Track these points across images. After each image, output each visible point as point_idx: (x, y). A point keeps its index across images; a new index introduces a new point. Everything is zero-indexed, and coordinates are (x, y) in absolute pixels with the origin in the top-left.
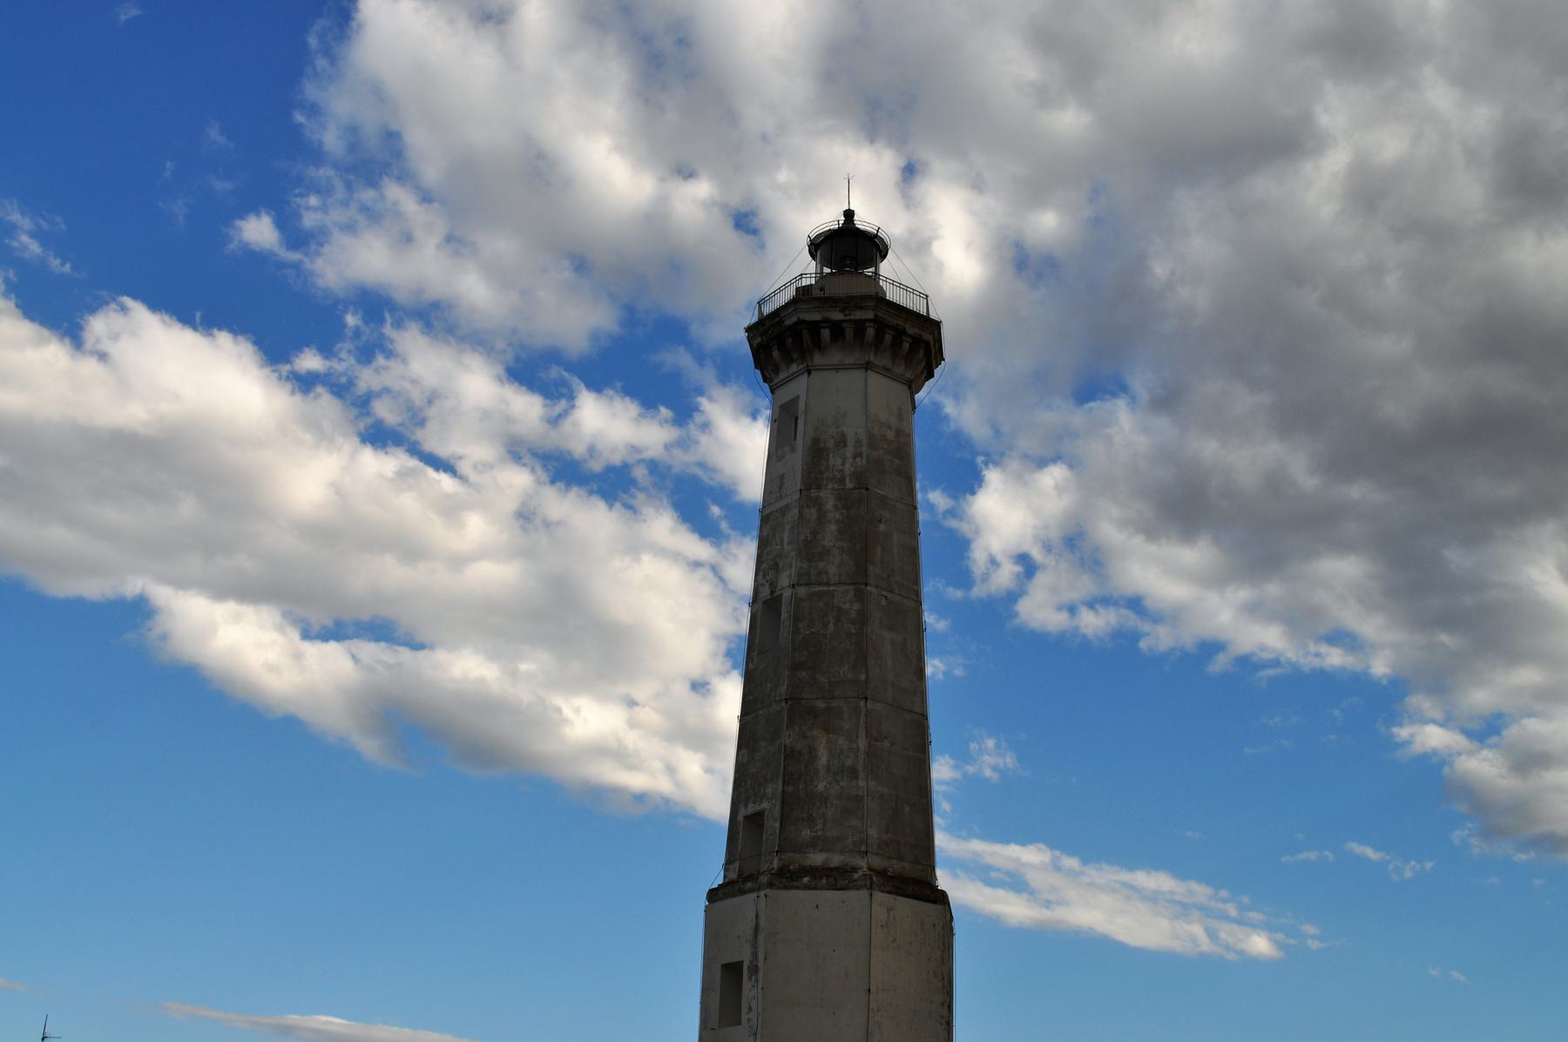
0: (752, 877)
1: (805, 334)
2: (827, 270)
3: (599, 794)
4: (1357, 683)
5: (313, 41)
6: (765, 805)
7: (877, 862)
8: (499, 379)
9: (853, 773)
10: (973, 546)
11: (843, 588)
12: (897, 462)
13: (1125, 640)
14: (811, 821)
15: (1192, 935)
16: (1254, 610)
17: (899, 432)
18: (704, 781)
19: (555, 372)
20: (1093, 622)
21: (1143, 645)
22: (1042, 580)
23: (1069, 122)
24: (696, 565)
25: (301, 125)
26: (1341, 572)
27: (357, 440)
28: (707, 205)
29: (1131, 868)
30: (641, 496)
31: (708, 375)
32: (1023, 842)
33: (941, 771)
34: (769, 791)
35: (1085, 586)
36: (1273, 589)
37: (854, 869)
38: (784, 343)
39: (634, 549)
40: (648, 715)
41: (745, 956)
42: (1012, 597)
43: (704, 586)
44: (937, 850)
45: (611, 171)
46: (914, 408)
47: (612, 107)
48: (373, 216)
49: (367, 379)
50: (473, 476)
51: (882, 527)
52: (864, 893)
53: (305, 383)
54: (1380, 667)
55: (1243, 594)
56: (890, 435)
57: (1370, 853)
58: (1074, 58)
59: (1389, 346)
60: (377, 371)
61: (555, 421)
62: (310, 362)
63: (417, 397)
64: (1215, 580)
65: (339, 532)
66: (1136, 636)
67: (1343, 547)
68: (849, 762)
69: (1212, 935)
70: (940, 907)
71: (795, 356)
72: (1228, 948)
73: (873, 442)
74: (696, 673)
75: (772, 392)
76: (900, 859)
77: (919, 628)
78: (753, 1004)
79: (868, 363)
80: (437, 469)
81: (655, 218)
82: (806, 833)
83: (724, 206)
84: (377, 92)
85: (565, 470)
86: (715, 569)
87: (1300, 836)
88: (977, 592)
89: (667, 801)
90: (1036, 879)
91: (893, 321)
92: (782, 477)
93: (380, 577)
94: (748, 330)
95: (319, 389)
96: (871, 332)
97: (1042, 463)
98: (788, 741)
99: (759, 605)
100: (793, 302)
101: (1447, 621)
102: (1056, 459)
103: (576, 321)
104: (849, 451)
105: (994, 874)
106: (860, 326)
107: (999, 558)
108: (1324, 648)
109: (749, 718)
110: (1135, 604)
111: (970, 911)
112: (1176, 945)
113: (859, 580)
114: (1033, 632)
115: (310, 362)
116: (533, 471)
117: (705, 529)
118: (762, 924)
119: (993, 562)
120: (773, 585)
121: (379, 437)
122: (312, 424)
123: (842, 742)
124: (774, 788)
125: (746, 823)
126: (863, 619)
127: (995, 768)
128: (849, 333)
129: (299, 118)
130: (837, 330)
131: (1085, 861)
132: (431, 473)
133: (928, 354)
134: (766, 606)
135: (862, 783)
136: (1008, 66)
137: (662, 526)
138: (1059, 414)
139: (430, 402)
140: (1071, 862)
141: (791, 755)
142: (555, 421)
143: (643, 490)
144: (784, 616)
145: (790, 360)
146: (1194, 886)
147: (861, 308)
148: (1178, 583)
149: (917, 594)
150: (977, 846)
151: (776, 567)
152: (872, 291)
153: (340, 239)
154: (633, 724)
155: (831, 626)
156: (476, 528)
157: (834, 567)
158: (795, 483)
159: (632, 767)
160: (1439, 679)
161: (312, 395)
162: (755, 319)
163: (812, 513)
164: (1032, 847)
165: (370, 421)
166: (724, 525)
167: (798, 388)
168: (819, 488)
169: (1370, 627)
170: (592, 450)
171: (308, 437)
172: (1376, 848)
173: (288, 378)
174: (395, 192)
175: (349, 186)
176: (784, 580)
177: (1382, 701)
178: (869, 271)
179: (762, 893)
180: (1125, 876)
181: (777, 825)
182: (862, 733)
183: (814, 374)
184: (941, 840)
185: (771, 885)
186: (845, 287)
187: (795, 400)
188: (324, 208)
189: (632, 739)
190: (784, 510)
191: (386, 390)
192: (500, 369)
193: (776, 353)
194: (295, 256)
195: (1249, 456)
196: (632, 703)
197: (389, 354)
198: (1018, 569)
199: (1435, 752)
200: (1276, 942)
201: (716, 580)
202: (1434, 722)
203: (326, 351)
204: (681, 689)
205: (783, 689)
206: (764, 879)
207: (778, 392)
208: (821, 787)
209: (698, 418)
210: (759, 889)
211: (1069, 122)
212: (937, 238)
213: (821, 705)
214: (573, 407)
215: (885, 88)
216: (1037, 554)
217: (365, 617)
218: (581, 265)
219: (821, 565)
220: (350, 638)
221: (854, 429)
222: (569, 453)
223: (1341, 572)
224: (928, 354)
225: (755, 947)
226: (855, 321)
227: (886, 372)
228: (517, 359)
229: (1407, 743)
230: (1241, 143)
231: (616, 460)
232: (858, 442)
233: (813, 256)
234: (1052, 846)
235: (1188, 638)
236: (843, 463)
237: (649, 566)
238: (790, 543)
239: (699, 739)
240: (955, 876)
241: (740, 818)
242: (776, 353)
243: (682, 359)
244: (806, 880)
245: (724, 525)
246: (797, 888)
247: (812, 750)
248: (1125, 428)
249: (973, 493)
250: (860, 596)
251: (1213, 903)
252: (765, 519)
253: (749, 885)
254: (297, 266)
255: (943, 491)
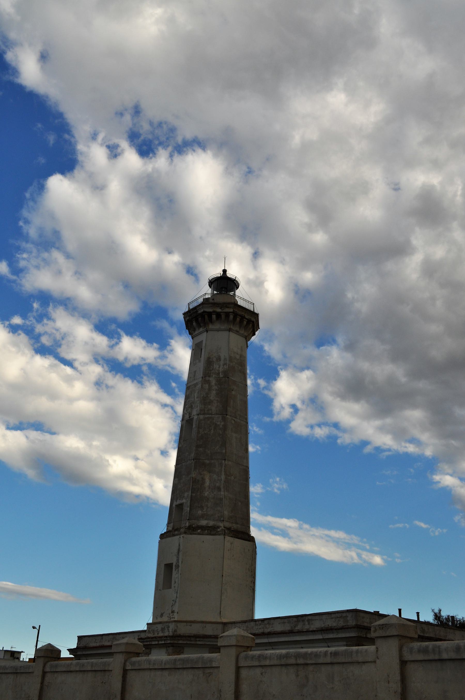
0: (177, 530)
1: (206, 317)
2: (215, 292)
3: (122, 494)
4: (420, 458)
5: (28, 195)
6: (184, 501)
7: (227, 525)
8: (91, 330)
9: (219, 489)
10: (275, 400)
11: (217, 416)
12: (240, 368)
13: (332, 439)
14: (202, 508)
15: (351, 556)
16: (381, 429)
17: (241, 356)
18: (161, 490)
19: (113, 327)
20: (320, 432)
21: (339, 441)
22: (301, 415)
23: (319, 238)
24: (165, 406)
25: (21, 227)
26: (415, 414)
27: (33, 352)
28: (176, 264)
29: (329, 529)
30: (145, 378)
31: (173, 331)
32: (288, 518)
33: (255, 489)
34: (186, 495)
35: (317, 418)
36: (389, 421)
37: (218, 527)
38: (198, 319)
39: (141, 398)
40: (142, 464)
41: (174, 561)
42: (289, 421)
43: (168, 413)
44: (251, 520)
45: (141, 249)
46: (247, 347)
47: (142, 225)
48: (47, 263)
49: (39, 328)
50: (80, 368)
51: (233, 393)
52: (222, 537)
53: (14, 329)
54: (428, 452)
55: (378, 423)
56: (238, 357)
57: (423, 525)
58: (322, 213)
59: (434, 328)
60: (43, 325)
61: (112, 347)
62: (17, 320)
63: (58, 337)
64: (367, 417)
65: (25, 387)
66: (336, 438)
67: (414, 406)
68: (217, 485)
69: (359, 555)
70: (251, 543)
71: (202, 325)
72: (365, 561)
73: (231, 359)
74: (162, 447)
75: (192, 338)
76: (237, 523)
77: (246, 433)
78: (177, 580)
79: (230, 329)
80: (65, 365)
81: (157, 269)
82: (200, 512)
83: (183, 264)
84: (52, 216)
85: (116, 366)
86: (172, 408)
87: (396, 518)
88: (275, 419)
89: (148, 498)
90: (292, 533)
91: (240, 313)
92: (195, 372)
93: (40, 405)
94: (184, 314)
95: (20, 332)
96: (231, 317)
97: (302, 369)
98: (194, 476)
99: (185, 422)
100: (202, 304)
101: (454, 435)
102: (308, 368)
103: (123, 308)
104: (222, 362)
105: (275, 530)
106: (227, 314)
107: (284, 406)
108: (407, 445)
109: (179, 466)
110: (336, 425)
111: (263, 543)
112: (345, 560)
113: (224, 413)
114: (297, 435)
115: (17, 320)
116: (103, 367)
117: (169, 391)
118: (181, 548)
119: (282, 407)
120: (190, 414)
121: (42, 351)
122: (15, 344)
123: (215, 476)
124: (188, 494)
125: (176, 508)
126: (225, 428)
127: (278, 489)
128: (223, 316)
129: (21, 223)
130: (218, 316)
131: (312, 526)
132: (62, 366)
133: (253, 326)
134: (187, 424)
135: (222, 493)
136: (297, 216)
137: (153, 389)
138: (311, 351)
139: (63, 339)
140: (306, 526)
141: (195, 481)
142: (112, 347)
143: (145, 375)
144: (194, 426)
145: (200, 326)
146: (354, 537)
147: (228, 307)
148: (352, 418)
149: (246, 419)
150: (270, 519)
151: (191, 407)
152: (233, 301)
153: (34, 271)
154: (137, 467)
155: (212, 431)
156: (79, 387)
157: (214, 408)
158: (200, 374)
159: (134, 484)
160: (449, 458)
161: (16, 334)
162: (187, 310)
163: (207, 386)
164: (291, 520)
165: (39, 345)
166: (177, 390)
167: (203, 337)
168: (209, 376)
169: (425, 437)
170: (126, 359)
171: (13, 349)
172: (426, 523)
173: (7, 327)
174: (57, 256)
175: (38, 251)
176: (195, 412)
177: (431, 465)
178: (232, 293)
179: (182, 536)
180: (327, 532)
181: (189, 509)
182: (223, 473)
183: (209, 332)
184: (254, 516)
185: (185, 533)
186: (222, 299)
187: (202, 342)
188: (28, 260)
189: (136, 473)
190: (195, 385)
191: (46, 333)
192: (92, 327)
193: (194, 324)
194: (14, 277)
195: (383, 370)
196: (136, 459)
197: (49, 318)
198: (291, 410)
199: (448, 486)
200: (382, 559)
201: (173, 412)
202: (448, 474)
203: (24, 317)
204: (157, 454)
205: (193, 455)
206: (182, 530)
207: (194, 338)
208: (206, 494)
209: (168, 348)
210: (180, 534)
211: (319, 238)
212: (267, 281)
213: (207, 462)
214: (120, 341)
215: (249, 223)
216: (299, 405)
217: (32, 421)
218: (127, 286)
219: (209, 406)
220: (26, 429)
221: (224, 354)
222: (117, 359)
223: (415, 414)
224: (253, 326)
225: (178, 558)
226: (226, 312)
227: (237, 332)
228: (100, 321)
229: (439, 482)
230: (381, 250)
231: (136, 363)
232: (225, 359)
233: (210, 287)
234: (299, 520)
235: (356, 439)
236: (219, 367)
237: (146, 405)
238: (197, 398)
239: (161, 474)
240: (260, 530)
241: (174, 506)
242: (194, 324)
243: (165, 324)
244: (199, 531)
245: (177, 390)
246: (195, 534)
247: (203, 479)
248: (335, 357)
249: (276, 380)
250: (224, 419)
251: (360, 543)
252: (188, 388)
253: (176, 532)
254: (14, 281)
255: (264, 379)
